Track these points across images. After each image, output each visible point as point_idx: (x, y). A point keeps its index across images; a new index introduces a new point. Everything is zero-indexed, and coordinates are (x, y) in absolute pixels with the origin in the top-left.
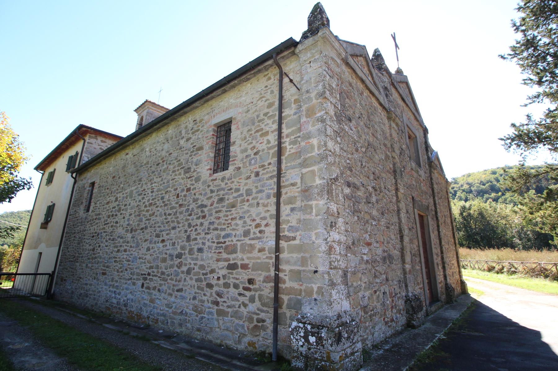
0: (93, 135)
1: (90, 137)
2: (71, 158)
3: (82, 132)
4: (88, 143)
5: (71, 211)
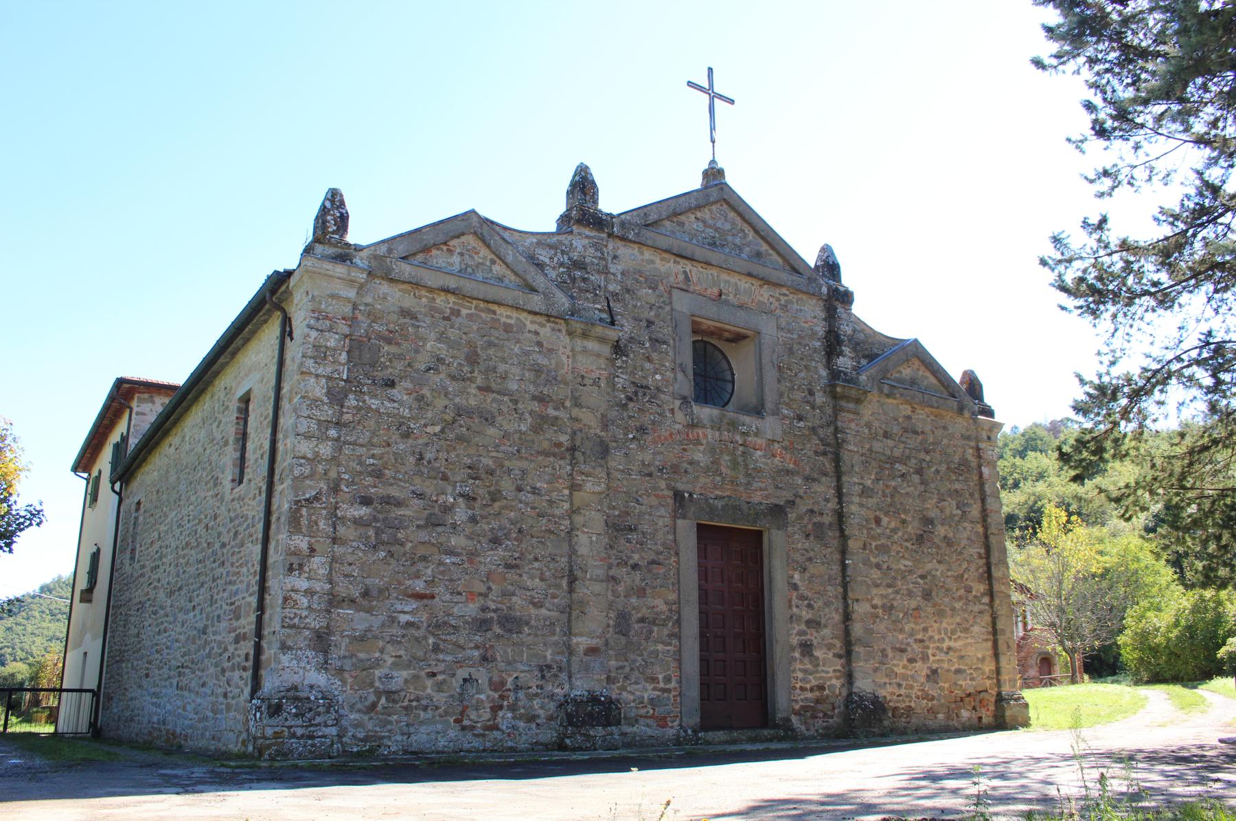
0: (146, 396)
1: (140, 400)
2: (117, 447)
3: (124, 393)
4: (137, 414)
5: (117, 566)
